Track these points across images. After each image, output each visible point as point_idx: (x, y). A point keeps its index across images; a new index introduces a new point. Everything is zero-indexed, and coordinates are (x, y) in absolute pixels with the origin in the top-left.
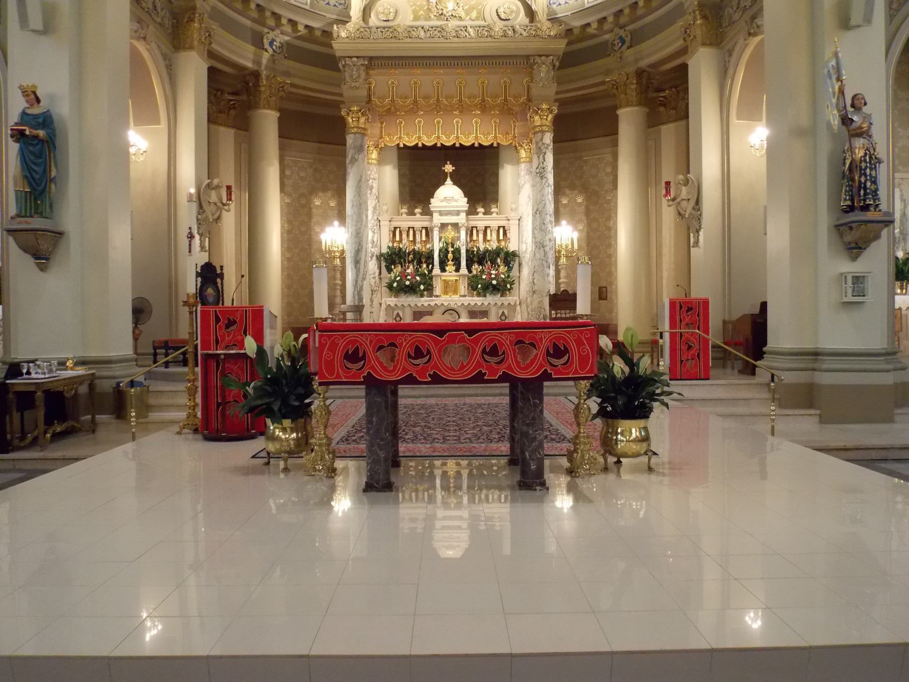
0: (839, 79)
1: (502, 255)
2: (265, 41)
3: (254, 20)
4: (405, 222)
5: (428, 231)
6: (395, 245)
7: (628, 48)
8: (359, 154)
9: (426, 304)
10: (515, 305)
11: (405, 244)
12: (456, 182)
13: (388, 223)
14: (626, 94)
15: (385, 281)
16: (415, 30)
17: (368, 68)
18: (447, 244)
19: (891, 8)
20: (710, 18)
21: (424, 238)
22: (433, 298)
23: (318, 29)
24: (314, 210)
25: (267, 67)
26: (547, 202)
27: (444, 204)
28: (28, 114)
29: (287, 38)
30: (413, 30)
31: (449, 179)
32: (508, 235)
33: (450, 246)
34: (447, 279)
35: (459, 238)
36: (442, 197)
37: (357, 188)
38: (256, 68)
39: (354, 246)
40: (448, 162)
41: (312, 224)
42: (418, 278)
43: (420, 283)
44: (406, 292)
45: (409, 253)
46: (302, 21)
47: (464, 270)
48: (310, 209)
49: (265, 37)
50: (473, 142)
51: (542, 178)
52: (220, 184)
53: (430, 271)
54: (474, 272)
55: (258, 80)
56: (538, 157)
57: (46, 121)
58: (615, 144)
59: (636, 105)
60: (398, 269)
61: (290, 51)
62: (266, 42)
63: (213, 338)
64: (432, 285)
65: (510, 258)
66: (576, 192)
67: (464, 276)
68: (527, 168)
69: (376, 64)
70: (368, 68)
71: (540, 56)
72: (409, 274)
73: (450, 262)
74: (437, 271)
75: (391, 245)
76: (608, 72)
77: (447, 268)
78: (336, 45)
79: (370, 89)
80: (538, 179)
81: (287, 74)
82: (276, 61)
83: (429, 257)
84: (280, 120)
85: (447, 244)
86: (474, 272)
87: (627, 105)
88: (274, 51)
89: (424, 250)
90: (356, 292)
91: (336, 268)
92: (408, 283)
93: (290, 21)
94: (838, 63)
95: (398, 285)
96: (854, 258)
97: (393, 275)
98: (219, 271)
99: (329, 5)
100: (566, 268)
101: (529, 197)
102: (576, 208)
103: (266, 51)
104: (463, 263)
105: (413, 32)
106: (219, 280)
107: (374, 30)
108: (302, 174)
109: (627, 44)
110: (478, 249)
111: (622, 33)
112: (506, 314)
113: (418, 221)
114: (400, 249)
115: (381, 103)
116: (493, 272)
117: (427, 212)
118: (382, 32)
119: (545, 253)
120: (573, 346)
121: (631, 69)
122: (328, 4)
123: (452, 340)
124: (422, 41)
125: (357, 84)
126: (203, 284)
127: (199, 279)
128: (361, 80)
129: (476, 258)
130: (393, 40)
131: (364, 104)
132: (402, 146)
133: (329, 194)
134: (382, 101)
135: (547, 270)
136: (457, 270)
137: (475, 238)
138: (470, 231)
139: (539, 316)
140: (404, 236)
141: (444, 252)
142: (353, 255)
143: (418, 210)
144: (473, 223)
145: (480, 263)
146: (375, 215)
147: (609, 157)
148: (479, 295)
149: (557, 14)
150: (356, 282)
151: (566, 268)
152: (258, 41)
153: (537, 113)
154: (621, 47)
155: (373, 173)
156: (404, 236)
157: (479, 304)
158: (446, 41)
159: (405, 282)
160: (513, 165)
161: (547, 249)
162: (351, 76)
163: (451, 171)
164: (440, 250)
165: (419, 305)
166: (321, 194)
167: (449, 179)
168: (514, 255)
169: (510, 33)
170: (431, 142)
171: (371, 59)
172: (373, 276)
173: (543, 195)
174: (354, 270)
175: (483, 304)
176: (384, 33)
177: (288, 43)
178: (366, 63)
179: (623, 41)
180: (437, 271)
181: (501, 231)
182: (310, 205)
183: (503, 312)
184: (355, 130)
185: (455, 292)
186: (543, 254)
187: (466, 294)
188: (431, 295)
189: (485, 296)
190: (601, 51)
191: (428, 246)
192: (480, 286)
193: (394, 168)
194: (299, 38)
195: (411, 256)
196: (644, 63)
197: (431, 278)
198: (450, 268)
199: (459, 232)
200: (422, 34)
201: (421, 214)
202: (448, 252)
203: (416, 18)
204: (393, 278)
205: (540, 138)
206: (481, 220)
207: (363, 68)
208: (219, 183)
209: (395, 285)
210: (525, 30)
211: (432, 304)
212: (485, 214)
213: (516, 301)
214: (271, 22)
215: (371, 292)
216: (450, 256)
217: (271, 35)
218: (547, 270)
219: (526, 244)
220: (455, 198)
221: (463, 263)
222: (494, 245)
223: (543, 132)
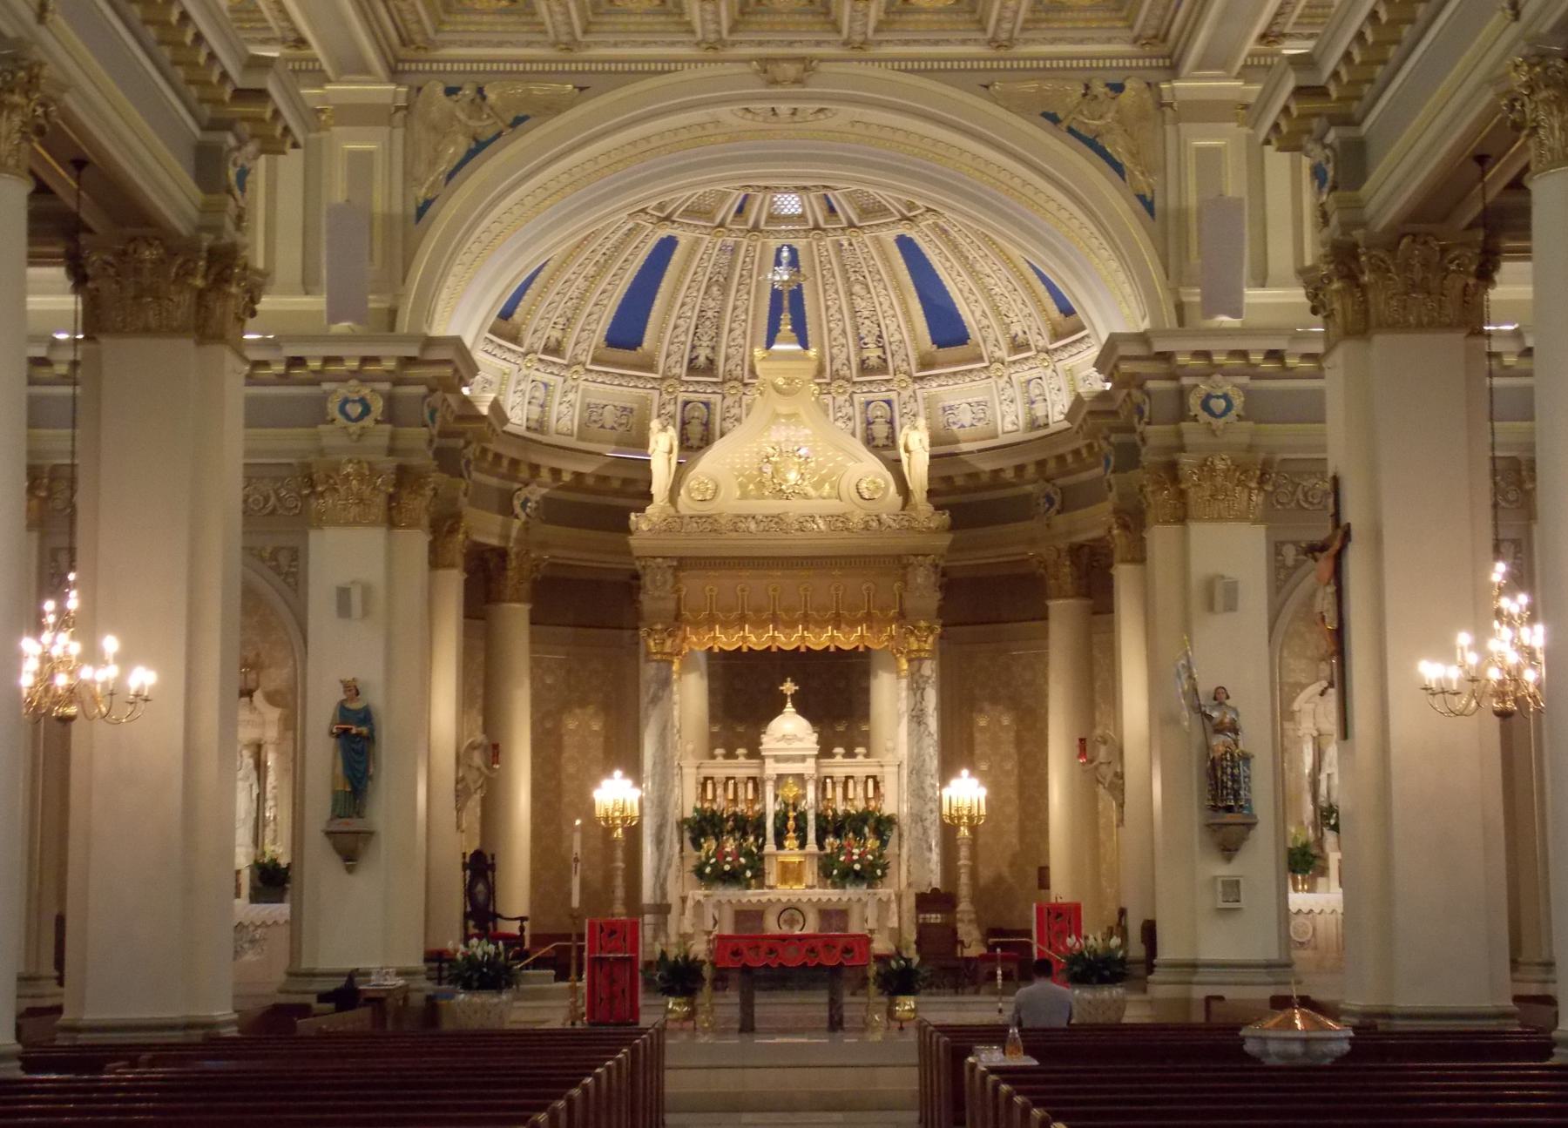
0: (1191, 677)
1: (871, 821)
4: (721, 768)
5: (757, 783)
6: (706, 805)
7: (1059, 512)
10: (889, 901)
11: (721, 804)
12: (803, 710)
13: (694, 770)
15: (691, 863)
17: (676, 569)
18: (787, 805)
19: (1277, 579)
20: (1132, 526)
21: (750, 796)
22: (766, 890)
24: (566, 738)
25: (518, 541)
26: (927, 758)
28: (349, 710)
29: (544, 491)
31: (789, 705)
32: (882, 790)
33: (791, 808)
34: (787, 860)
35: (804, 796)
36: (779, 735)
38: (503, 544)
41: (563, 761)
42: (742, 860)
43: (745, 867)
44: (724, 882)
45: (727, 819)
47: (812, 846)
48: (560, 737)
51: (919, 723)
53: (761, 848)
54: (828, 850)
55: (504, 561)
57: (366, 717)
59: (1072, 597)
60: (710, 845)
61: (552, 511)
62: (517, 503)
63: (598, 944)
64: (763, 870)
65: (883, 826)
66: (1000, 707)
67: (811, 855)
70: (676, 569)
71: (916, 555)
72: (728, 854)
73: (791, 834)
74: (770, 847)
75: (699, 805)
76: (1032, 542)
77: (787, 843)
78: (633, 541)
79: (679, 599)
80: (914, 725)
83: (759, 826)
85: (787, 805)
86: (828, 850)
87: (1059, 597)
88: (527, 515)
89: (750, 813)
92: (727, 867)
94: (1188, 661)
95: (712, 871)
96: (1229, 859)
97: (703, 853)
98: (490, 861)
103: (517, 517)
104: (811, 835)
106: (490, 873)
107: (686, 520)
108: (549, 681)
109: (1057, 506)
110: (835, 811)
111: (1049, 488)
113: (741, 767)
114: (713, 812)
116: (856, 851)
117: (755, 753)
119: (925, 830)
120: (856, 948)
122: (602, 427)
123: (790, 944)
125: (663, 594)
126: (473, 878)
127: (468, 872)
128: (668, 587)
129: (831, 826)
130: (713, 534)
132: (716, 650)
133: (591, 710)
135: (928, 854)
136: (802, 845)
137: (829, 795)
138: (821, 785)
140: (720, 791)
141: (781, 818)
143: (741, 751)
144: (826, 771)
145: (837, 835)
148: (834, 886)
149: (958, 442)
152: (507, 510)
153: (912, 632)
154: (1048, 509)
156: (720, 791)
157: (834, 899)
158: (784, 536)
161: (927, 824)
162: (654, 581)
164: (776, 815)
165: (745, 900)
166: (578, 711)
167: (789, 705)
168: (890, 821)
169: (874, 524)
171: (681, 559)
173: (920, 749)
174: (656, 854)
177: (545, 498)
179: (1051, 502)
181: (871, 782)
184: (659, 657)
185: (799, 880)
186: (921, 830)
187: (816, 882)
188: (761, 885)
189: (844, 887)
190: (1019, 509)
191: (757, 807)
192: (835, 872)
193: (701, 676)
195: (731, 823)
196: (1081, 538)
197: (762, 859)
198: (791, 843)
199: (804, 787)
200: (753, 526)
202: (788, 818)
203: (745, 496)
204: (703, 859)
206: (839, 766)
207: (671, 571)
209: (708, 870)
211: (764, 899)
212: (845, 756)
213: (890, 895)
216: (791, 824)
217: (525, 493)
218: (927, 854)
220: (800, 736)
221: (811, 835)
222: (860, 805)
223: (921, 660)
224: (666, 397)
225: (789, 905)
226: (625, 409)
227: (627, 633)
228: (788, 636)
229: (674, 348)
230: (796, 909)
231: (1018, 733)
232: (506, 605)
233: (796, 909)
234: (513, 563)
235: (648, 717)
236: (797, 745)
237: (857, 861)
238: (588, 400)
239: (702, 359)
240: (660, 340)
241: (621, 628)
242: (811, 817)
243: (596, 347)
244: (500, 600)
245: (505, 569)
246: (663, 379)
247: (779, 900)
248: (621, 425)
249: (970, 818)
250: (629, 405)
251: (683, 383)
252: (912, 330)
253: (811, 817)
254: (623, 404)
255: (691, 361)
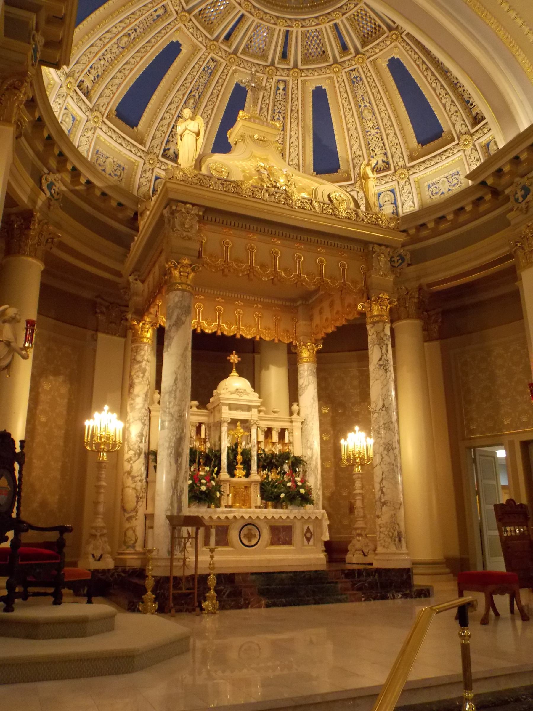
2: (43, 181)
3: (37, 153)
7: (409, 265)
8: (186, 316)
9: (277, 517)
14: (406, 307)
16: (260, 191)
23: (99, 188)
24: (42, 395)
27: (235, 396)
29: (64, 188)
30: (258, 191)
37: (182, 357)
38: (30, 206)
39: (175, 433)
40: (234, 352)
41: (38, 412)
46: (86, 175)
49: (44, 177)
50: (254, 335)
52: (18, 317)
56: (381, 348)
58: (365, 359)
68: (310, 368)
69: (210, 219)
73: (239, 466)
74: (224, 475)
81: (58, 225)
82: (52, 207)
84: (44, 273)
90: (175, 497)
91: (103, 465)
93: (74, 169)
99: (105, 172)
100: (362, 478)
101: (313, 399)
102: (518, 397)
105: (257, 193)
106: (16, 466)
112: (311, 529)
115: (213, 262)
118: (223, 184)
121: (415, 284)
124: (266, 203)
131: (195, 258)
133: (61, 379)
134: (214, 260)
136: (248, 475)
139: (393, 534)
141: (233, 451)
142: (173, 444)
146: (146, 403)
147: (354, 371)
150: (176, 482)
151: (362, 478)
155: (147, 354)
159: (200, 487)
160: (279, 367)
163: (237, 362)
164: (229, 448)
166: (51, 378)
170: (211, 329)
171: (207, 210)
172: (139, 478)
174: (174, 466)
175: (288, 517)
176: (225, 186)
178: (201, 213)
180: (224, 475)
182: (38, 388)
183: (308, 528)
186: (393, 458)
192: (282, 495)
194: (74, 192)
196: (425, 281)
198: (240, 472)
201: (198, 407)
205: (381, 329)
208: (16, 314)
210: (366, 217)
211: (230, 516)
214: (53, 163)
215: (136, 499)
219: (312, 449)
224: (148, 166)
225: (250, 521)
226: (119, 166)
227: (90, 333)
228: (230, 325)
229: (158, 134)
230: (254, 525)
231: (333, 417)
232: (24, 258)
233: (254, 525)
234: (35, 226)
235: (171, 338)
236: (245, 397)
237: (301, 487)
238: (97, 147)
239: (171, 151)
240: (150, 126)
241: (86, 328)
242: (254, 453)
243: (110, 111)
244: (20, 252)
245: (28, 228)
246: (147, 153)
247: (242, 517)
248: (116, 175)
249: (362, 459)
250: (122, 164)
251: (159, 161)
252: (304, 159)
253: (254, 453)
254: (119, 162)
255: (165, 150)
